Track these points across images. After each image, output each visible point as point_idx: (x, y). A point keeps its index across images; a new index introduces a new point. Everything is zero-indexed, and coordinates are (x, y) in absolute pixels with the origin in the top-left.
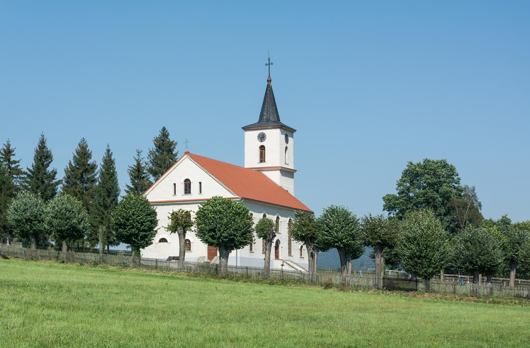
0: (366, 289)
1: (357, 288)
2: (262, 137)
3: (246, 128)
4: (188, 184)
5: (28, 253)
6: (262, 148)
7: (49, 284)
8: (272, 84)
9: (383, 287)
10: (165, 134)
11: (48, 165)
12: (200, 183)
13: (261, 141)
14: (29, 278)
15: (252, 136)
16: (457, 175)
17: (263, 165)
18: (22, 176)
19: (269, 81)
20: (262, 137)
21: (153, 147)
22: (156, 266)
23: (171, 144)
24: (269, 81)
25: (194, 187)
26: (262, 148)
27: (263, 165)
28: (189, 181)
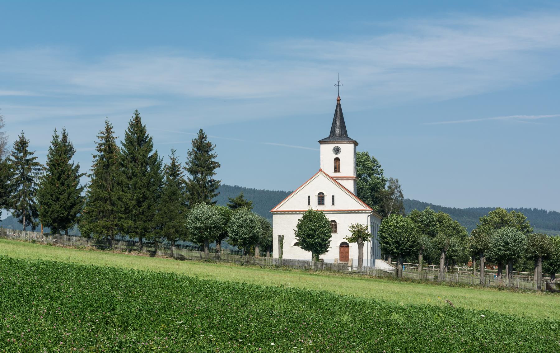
0: (534, 291)
1: (524, 290)
2: (337, 150)
3: (322, 142)
4: (321, 198)
5: (203, 256)
6: (337, 160)
7: (188, 279)
8: (341, 102)
9: (546, 290)
10: (202, 136)
11: (70, 157)
12: (333, 197)
13: (336, 154)
14: (362, 284)
15: (327, 151)
16: (380, 167)
17: (337, 175)
18: (36, 168)
19: (339, 100)
20: (337, 150)
21: (190, 147)
22: (329, 269)
23: (209, 145)
24: (339, 100)
25: (328, 200)
26: (337, 160)
27: (337, 175)
28: (323, 194)
